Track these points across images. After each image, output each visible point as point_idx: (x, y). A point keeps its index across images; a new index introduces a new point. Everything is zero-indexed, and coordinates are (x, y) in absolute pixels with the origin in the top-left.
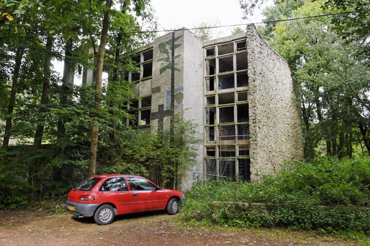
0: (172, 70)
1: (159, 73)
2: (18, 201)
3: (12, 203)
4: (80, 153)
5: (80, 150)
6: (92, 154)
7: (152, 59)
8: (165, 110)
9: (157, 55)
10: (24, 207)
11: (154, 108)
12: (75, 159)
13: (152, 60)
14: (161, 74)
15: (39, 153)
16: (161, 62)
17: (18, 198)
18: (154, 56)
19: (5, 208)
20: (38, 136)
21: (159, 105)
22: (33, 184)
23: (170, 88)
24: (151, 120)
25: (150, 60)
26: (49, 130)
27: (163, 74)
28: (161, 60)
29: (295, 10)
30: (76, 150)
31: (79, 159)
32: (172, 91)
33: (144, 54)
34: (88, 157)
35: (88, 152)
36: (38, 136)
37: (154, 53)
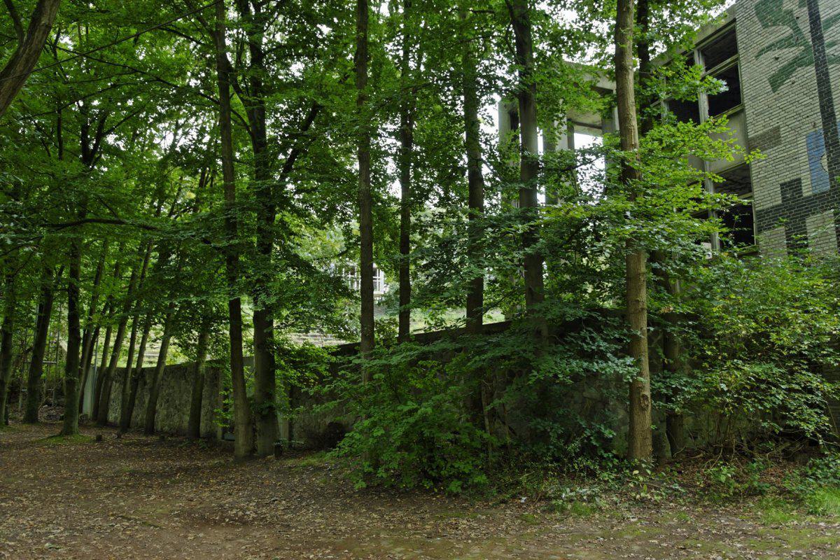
0: (817, 66)
1: (769, 88)
2: (464, 473)
3: (450, 478)
4: (602, 338)
5: (599, 331)
6: (636, 339)
7: (734, 57)
8: (807, 192)
9: (750, 38)
10: (479, 491)
11: (765, 196)
12: (590, 356)
13: (737, 59)
14: (774, 90)
15: (498, 345)
16: (771, 54)
17: (460, 465)
18: (740, 46)
19: (436, 490)
20: (475, 306)
21: (782, 185)
22: (488, 428)
23: (820, 122)
24: (760, 231)
25: (729, 60)
26: (497, 285)
27: (783, 88)
28: (769, 48)
29: (690, 125)
30: (590, 332)
31: (602, 356)
32: (826, 133)
33: (703, 52)
34: (627, 348)
35: (625, 335)
36: (475, 306)
37: (739, 37)
